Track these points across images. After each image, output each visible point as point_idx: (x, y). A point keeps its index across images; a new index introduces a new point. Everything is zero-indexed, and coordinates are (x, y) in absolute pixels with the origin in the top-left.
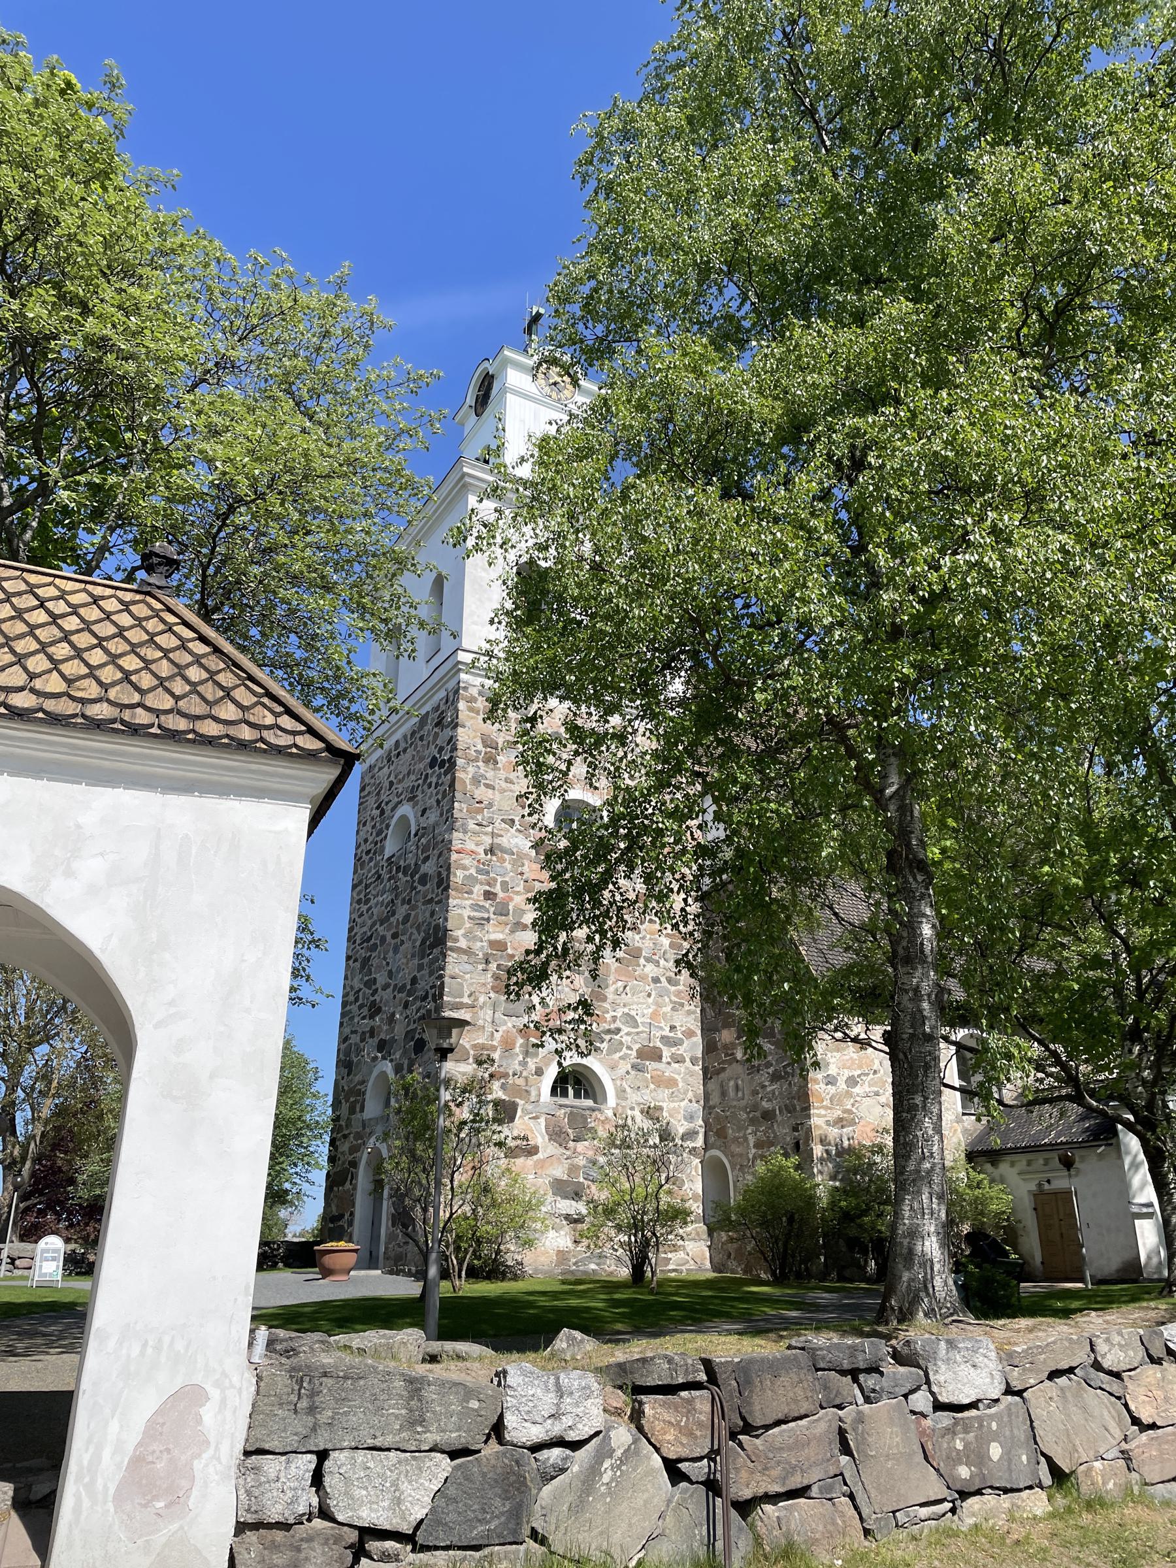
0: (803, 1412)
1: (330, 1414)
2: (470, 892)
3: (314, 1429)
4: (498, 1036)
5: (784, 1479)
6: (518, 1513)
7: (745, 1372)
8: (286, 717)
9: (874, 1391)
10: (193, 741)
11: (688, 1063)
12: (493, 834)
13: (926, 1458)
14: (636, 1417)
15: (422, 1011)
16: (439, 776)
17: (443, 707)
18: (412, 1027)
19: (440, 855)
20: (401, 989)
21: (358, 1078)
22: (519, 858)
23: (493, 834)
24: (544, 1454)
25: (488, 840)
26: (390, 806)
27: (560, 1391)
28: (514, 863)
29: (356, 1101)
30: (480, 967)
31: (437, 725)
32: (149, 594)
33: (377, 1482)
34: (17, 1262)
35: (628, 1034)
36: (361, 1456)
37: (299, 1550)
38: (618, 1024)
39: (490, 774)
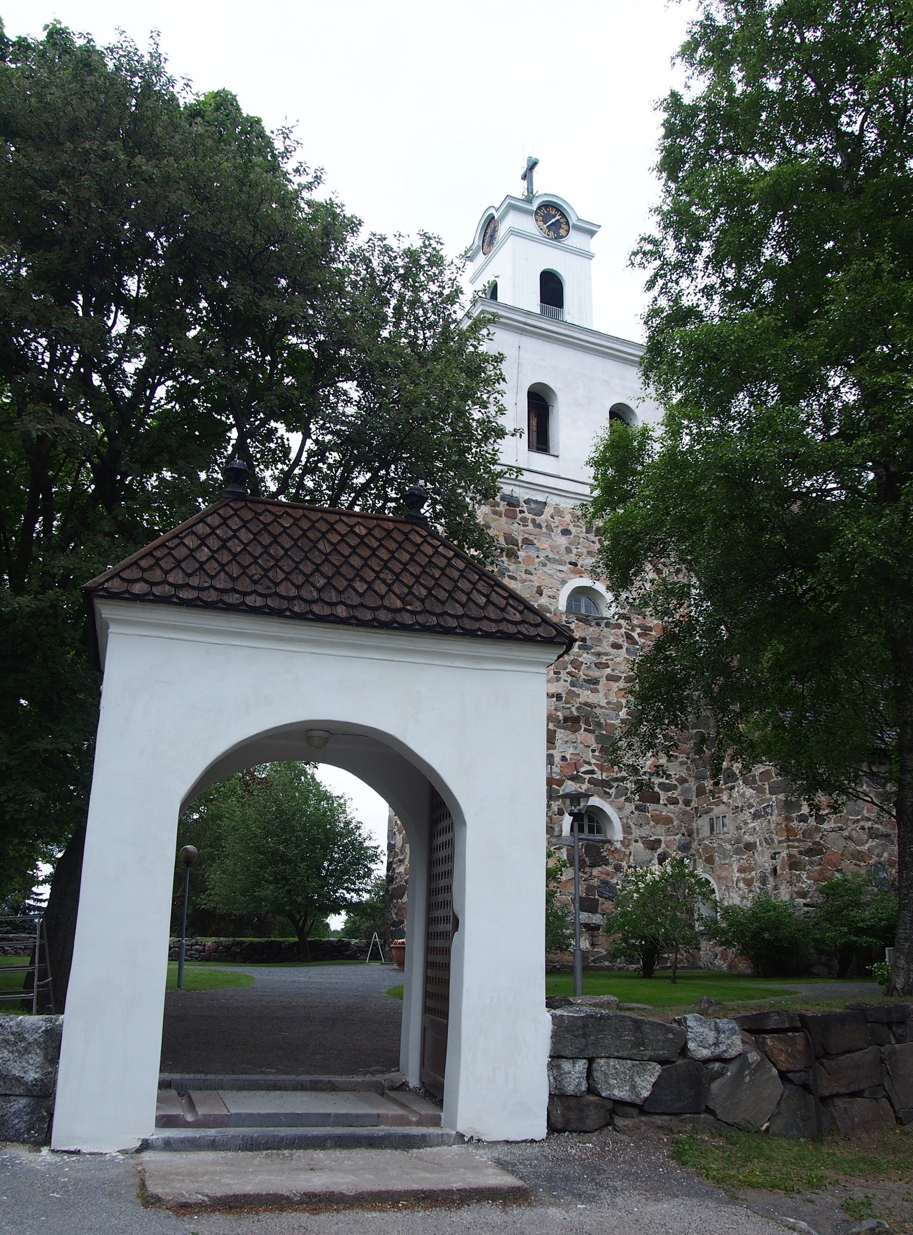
1: (593, 1038)
3: (586, 1046)
9: (902, 1036)
11: (681, 805)
24: (711, 1066)
27: (718, 1030)
33: (622, 1076)
36: (612, 1062)
37: (582, 1111)
39: (512, 567)
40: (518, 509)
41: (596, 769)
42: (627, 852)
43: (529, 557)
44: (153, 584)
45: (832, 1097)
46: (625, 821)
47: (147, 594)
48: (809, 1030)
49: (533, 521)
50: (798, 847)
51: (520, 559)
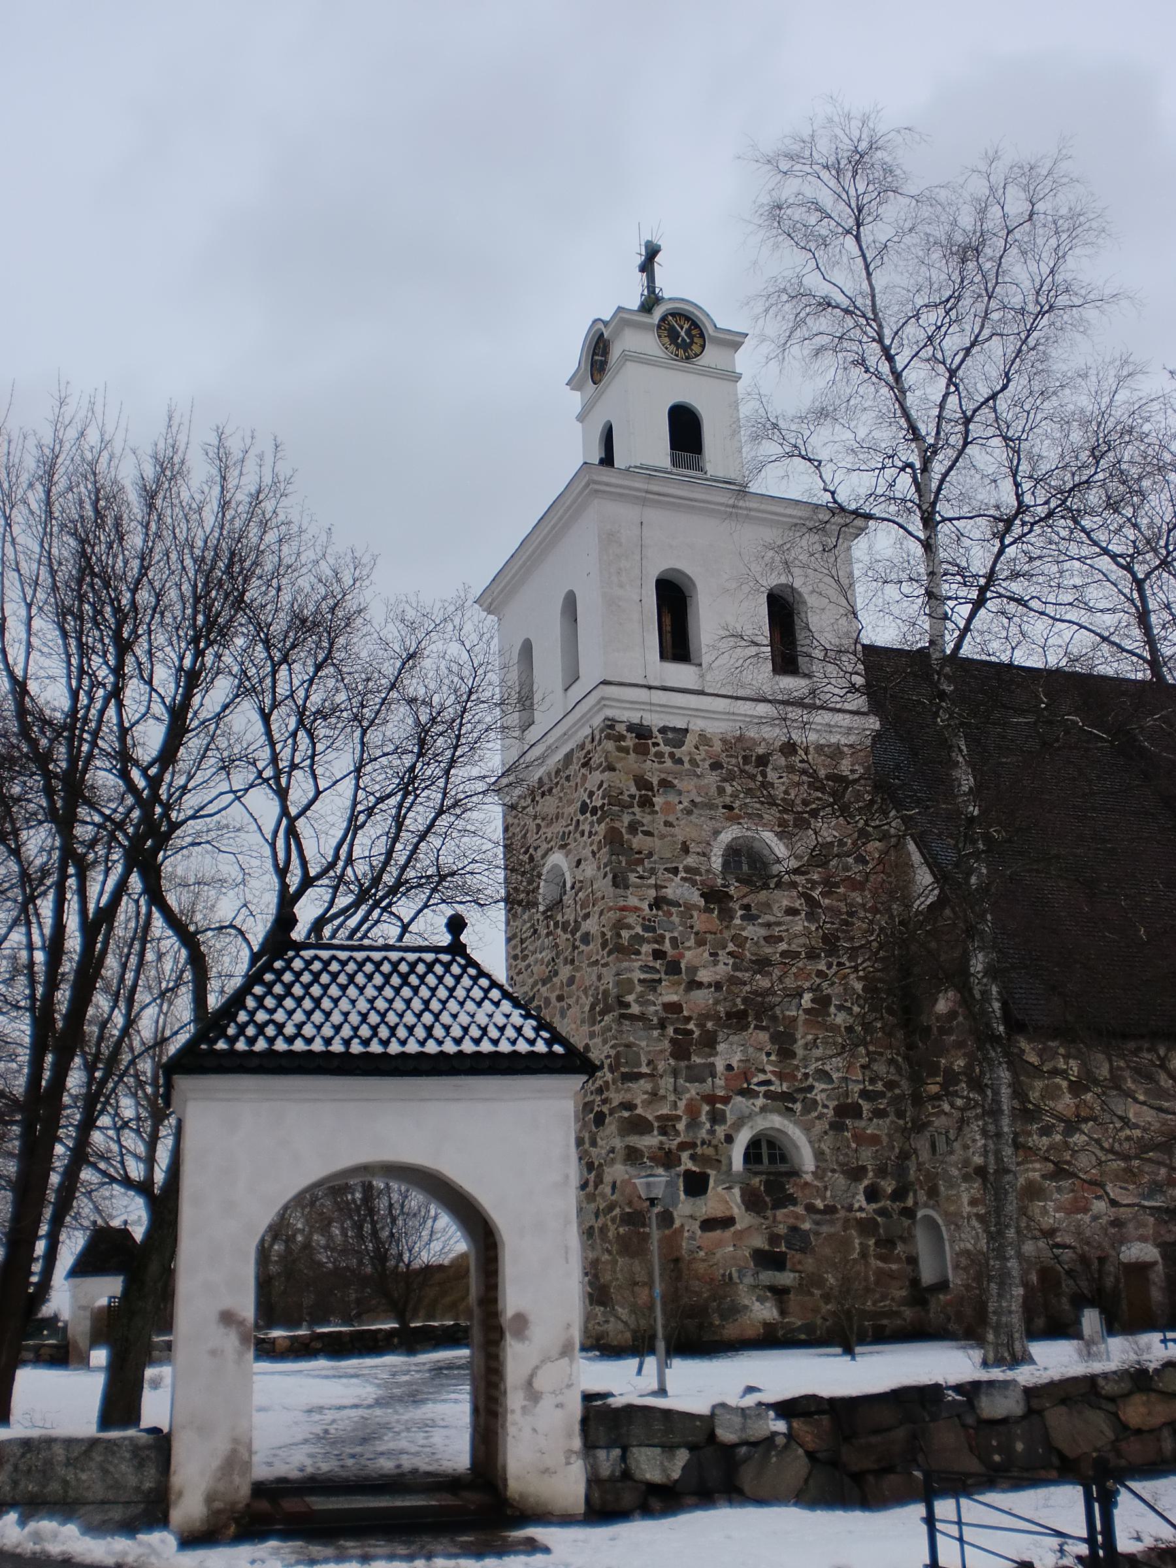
4: (682, 1105)
16: (592, 824)
17: (589, 747)
18: (589, 1098)
23: (657, 887)
25: (652, 893)
26: (540, 852)
28: (682, 915)
31: (584, 765)
39: (647, 819)
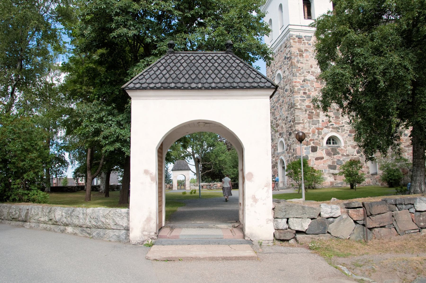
0: (384, 212)
2: (299, 93)
3: (286, 214)
4: (311, 130)
5: (380, 224)
6: (325, 228)
7: (371, 204)
8: (262, 78)
10: (246, 88)
12: (304, 76)
13: (413, 221)
14: (348, 213)
15: (290, 125)
19: (290, 84)
20: (284, 120)
21: (275, 143)
22: (312, 82)
23: (304, 76)
24: (329, 219)
25: (303, 78)
26: (275, 71)
27: (332, 209)
28: (311, 83)
29: (275, 148)
30: (304, 113)
31: (285, 47)
32: (228, 53)
33: (298, 223)
34: (203, 187)
35: (346, 127)
37: (285, 234)
38: (343, 124)
39: (301, 59)
40: (302, 40)
41: (334, 124)
42: (346, 150)
43: (307, 55)
44: (142, 84)
45: (373, 228)
46: (344, 140)
47: (140, 87)
48: (365, 207)
49: (308, 43)
50: (404, 145)
51: (304, 56)
